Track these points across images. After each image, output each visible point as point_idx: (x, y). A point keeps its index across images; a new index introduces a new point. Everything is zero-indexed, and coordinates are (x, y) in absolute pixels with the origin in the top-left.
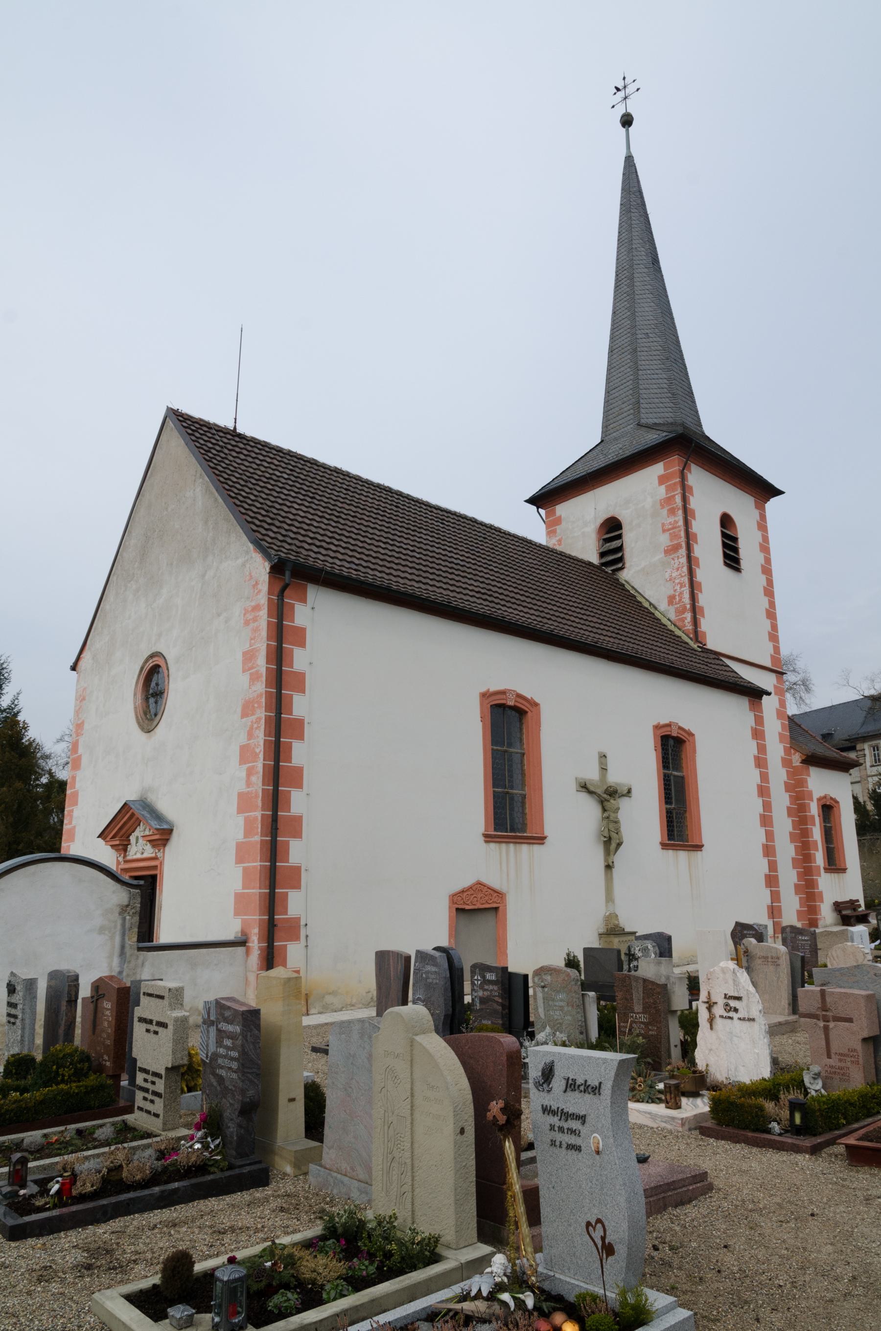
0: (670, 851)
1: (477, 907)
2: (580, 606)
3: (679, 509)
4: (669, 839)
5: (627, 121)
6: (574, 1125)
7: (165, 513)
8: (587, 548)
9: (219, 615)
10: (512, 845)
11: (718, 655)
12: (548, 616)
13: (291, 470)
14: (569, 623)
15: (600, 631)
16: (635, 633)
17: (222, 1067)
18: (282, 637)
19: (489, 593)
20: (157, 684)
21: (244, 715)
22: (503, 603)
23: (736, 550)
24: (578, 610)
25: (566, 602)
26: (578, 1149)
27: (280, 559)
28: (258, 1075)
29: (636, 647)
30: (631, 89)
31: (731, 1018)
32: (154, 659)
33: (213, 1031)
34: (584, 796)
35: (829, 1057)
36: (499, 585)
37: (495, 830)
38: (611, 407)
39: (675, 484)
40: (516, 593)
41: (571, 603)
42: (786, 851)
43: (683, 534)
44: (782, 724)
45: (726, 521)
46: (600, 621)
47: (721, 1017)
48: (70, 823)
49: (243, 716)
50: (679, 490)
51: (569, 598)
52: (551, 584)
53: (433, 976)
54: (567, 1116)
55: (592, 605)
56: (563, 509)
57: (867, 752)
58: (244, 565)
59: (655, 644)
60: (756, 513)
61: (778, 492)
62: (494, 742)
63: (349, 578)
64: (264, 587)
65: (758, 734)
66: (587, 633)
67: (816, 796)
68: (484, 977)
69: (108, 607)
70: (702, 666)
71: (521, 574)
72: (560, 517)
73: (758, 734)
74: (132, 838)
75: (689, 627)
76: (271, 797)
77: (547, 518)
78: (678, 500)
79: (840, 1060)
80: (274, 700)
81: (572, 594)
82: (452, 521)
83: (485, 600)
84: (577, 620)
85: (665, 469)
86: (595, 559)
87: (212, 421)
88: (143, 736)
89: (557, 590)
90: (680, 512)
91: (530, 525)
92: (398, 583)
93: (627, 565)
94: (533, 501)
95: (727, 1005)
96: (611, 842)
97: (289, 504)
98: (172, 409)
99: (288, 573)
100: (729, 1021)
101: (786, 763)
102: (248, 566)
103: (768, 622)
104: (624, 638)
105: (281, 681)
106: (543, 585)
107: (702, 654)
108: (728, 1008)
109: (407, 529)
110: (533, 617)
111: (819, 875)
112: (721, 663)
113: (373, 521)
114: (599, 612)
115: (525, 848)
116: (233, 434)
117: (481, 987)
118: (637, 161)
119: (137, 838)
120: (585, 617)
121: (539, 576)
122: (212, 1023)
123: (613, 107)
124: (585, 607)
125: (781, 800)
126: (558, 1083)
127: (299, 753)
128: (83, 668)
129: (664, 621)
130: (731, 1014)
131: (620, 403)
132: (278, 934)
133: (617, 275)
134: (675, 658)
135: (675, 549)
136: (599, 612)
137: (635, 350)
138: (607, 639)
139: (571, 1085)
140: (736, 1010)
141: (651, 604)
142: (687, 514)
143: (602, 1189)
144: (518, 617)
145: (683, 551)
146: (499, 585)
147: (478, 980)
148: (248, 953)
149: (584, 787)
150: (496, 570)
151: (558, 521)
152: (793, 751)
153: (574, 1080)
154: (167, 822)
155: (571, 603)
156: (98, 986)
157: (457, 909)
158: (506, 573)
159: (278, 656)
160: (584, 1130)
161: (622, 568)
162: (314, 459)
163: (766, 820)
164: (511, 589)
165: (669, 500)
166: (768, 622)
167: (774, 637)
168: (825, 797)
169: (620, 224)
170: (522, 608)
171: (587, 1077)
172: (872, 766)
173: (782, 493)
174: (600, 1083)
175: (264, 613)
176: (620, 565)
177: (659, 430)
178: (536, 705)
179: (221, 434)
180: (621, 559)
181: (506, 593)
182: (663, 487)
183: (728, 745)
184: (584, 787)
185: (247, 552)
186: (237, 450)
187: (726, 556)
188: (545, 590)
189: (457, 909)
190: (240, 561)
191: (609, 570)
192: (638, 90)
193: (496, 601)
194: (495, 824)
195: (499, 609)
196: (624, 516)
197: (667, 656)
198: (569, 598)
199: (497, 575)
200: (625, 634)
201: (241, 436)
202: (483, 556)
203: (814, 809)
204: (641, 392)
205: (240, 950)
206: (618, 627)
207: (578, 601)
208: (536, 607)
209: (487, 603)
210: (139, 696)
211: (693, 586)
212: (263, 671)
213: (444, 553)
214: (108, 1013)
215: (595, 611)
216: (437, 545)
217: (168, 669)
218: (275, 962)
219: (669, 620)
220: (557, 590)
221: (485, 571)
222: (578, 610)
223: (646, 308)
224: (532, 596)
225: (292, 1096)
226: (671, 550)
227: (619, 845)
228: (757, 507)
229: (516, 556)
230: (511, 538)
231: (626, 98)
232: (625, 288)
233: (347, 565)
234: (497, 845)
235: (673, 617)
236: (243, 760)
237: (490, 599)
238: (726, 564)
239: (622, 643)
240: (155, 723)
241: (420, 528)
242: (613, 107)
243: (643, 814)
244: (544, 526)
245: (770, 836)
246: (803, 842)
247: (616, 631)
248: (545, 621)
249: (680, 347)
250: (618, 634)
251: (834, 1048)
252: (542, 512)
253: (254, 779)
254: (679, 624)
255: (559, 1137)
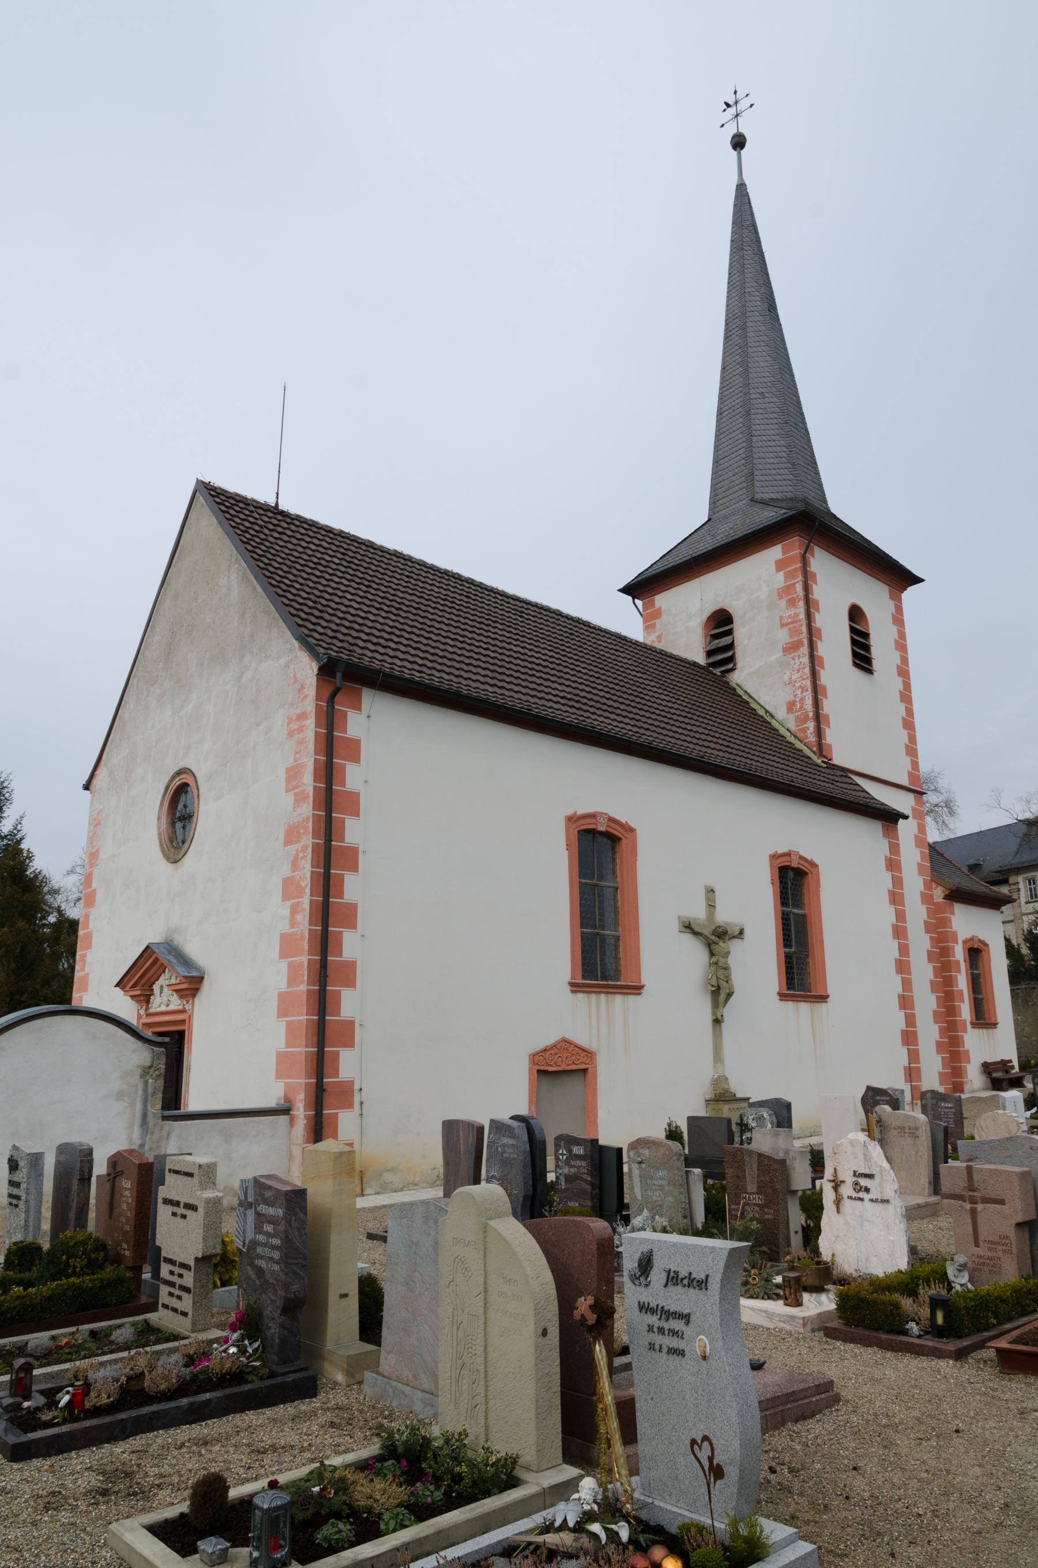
0: (790, 1003)
1: (562, 1069)
2: (684, 714)
3: (799, 600)
4: (788, 989)
5: (739, 143)
6: (677, 1325)
7: (195, 604)
8: (691, 646)
9: (258, 725)
10: (603, 996)
11: (845, 771)
12: (646, 726)
13: (343, 554)
14: (671, 734)
15: (706, 744)
16: (749, 746)
17: (262, 1257)
18: (332, 751)
19: (577, 698)
20: (185, 806)
21: (288, 842)
22: (592, 710)
23: (867, 648)
24: (681, 719)
25: (667, 709)
26: (681, 1353)
27: (330, 658)
28: (304, 1266)
29: (749, 762)
30: (743, 105)
31: (861, 1199)
32: (182, 776)
33: (251, 1214)
34: (688, 938)
35: (977, 1245)
36: (588, 689)
37: (584, 978)
38: (720, 479)
39: (795, 570)
40: (608, 699)
41: (673, 711)
42: (926, 1003)
43: (804, 629)
44: (922, 853)
45: (856, 614)
46: (706, 732)
47: (850, 1198)
48: (83, 969)
49: (286, 844)
50: (800, 578)
51: (670, 704)
52: (649, 688)
53: (510, 1150)
54: (668, 1315)
55: (698, 713)
56: (663, 600)
57: (1021, 886)
58: (287, 666)
59: (772, 758)
60: (891, 605)
61: (917, 580)
62: (582, 874)
63: (411, 681)
64: (311, 692)
65: (893, 865)
66: (691, 746)
67: (961, 938)
68: (570, 1151)
69: (127, 715)
70: (827, 785)
71: (614, 676)
72: (660, 609)
73: (893, 865)
74: (156, 988)
75: (812, 739)
76: (319, 939)
77: (644, 610)
78: (799, 589)
79: (990, 1249)
80: (323, 825)
81: (673, 700)
82: (533, 614)
83: (572, 707)
84: (680, 731)
85: (784, 553)
86: (701, 659)
87: (250, 496)
88: (169, 867)
89: (657, 695)
90: (801, 603)
91: (624, 619)
92: (469, 687)
93: (739, 665)
94: (628, 590)
95: (856, 1184)
96: (720, 992)
97: (340, 594)
98: (203, 482)
99: (339, 675)
100: (859, 1203)
101: (926, 898)
102: (292, 667)
103: (905, 733)
104: (735, 752)
105: (331, 802)
106: (639, 690)
107: (827, 771)
108: (857, 1187)
109: (480, 623)
110: (628, 727)
111: (965, 1031)
112: (850, 781)
113: (440, 613)
114: (706, 721)
115: (618, 999)
116: (275, 511)
117: (567, 1163)
118: (750, 190)
119: (162, 987)
120: (689, 727)
121: (635, 679)
122: (250, 1205)
123: (722, 126)
124: (690, 716)
125: (920, 943)
126: (657, 1276)
127: (353, 888)
128: (98, 787)
129: (783, 731)
130: (862, 1195)
131: (730, 474)
132: (327, 1100)
133: (727, 324)
134: (795, 776)
135: (795, 646)
136: (706, 721)
137: (748, 413)
138: (716, 752)
139: (673, 1279)
140: (867, 1190)
141: (767, 711)
142: (810, 605)
143: (709, 1400)
144: (610, 727)
145: (805, 650)
146: (588, 689)
147: (563, 1154)
148: (292, 1122)
149: (688, 927)
150: (584, 671)
151: (658, 614)
152: (934, 885)
153: (676, 1273)
154: (197, 969)
155: (673, 711)
156: (115, 1162)
157: (539, 1071)
158: (596, 675)
159: (328, 773)
160: (688, 1331)
161: (733, 670)
162: (369, 541)
163: (902, 967)
164: (602, 694)
165: (788, 589)
166: (905, 732)
167: (911, 750)
168: (972, 939)
169: (730, 264)
170: (615, 717)
171: (692, 1269)
172: (1027, 903)
173: (922, 580)
174: (707, 1276)
175: (310, 723)
176: (730, 666)
177: (776, 507)
178: (632, 830)
179: (261, 512)
180: (731, 659)
181: (596, 698)
182: (781, 573)
183: (858, 878)
184: (688, 927)
185: (291, 651)
186: (280, 530)
187: (855, 655)
188: (642, 695)
189: (539, 1071)
190: (283, 661)
191: (717, 671)
192: (752, 106)
193: (585, 708)
194: (584, 970)
195: (588, 718)
196: (735, 608)
197: (785, 773)
198: (670, 704)
199: (585, 677)
200: (737, 747)
201: (284, 514)
202: (569, 655)
203: (959, 954)
204: (755, 461)
205: (283, 1119)
206: (728, 739)
207: (681, 708)
208: (631, 716)
209: (574, 710)
210: (164, 820)
211: (817, 691)
212: (310, 790)
213: (523, 651)
214: (127, 1193)
215: (701, 720)
216: (515, 643)
217: (198, 788)
218: (324, 1133)
219: (788, 730)
220: (657, 695)
221: (572, 672)
222: (681, 719)
223: (762, 363)
224: (627, 702)
225: (344, 1291)
226: (791, 648)
227: (729, 995)
228: (891, 598)
229: (608, 655)
230: (602, 634)
231: (737, 115)
232: (736, 340)
233: (409, 666)
234: (586, 995)
235: (793, 727)
236: (286, 895)
237: (577, 705)
238: (856, 665)
239: (733, 757)
240: (183, 852)
241: (494, 622)
242: (722, 126)
243: (758, 959)
244: (641, 619)
245: (907, 984)
246: (946, 992)
247: (726, 743)
248: (642, 731)
249: (801, 408)
250: (728, 746)
251: (983, 1234)
252: (639, 603)
253: (299, 917)
254: (800, 735)
255: (659, 1339)
